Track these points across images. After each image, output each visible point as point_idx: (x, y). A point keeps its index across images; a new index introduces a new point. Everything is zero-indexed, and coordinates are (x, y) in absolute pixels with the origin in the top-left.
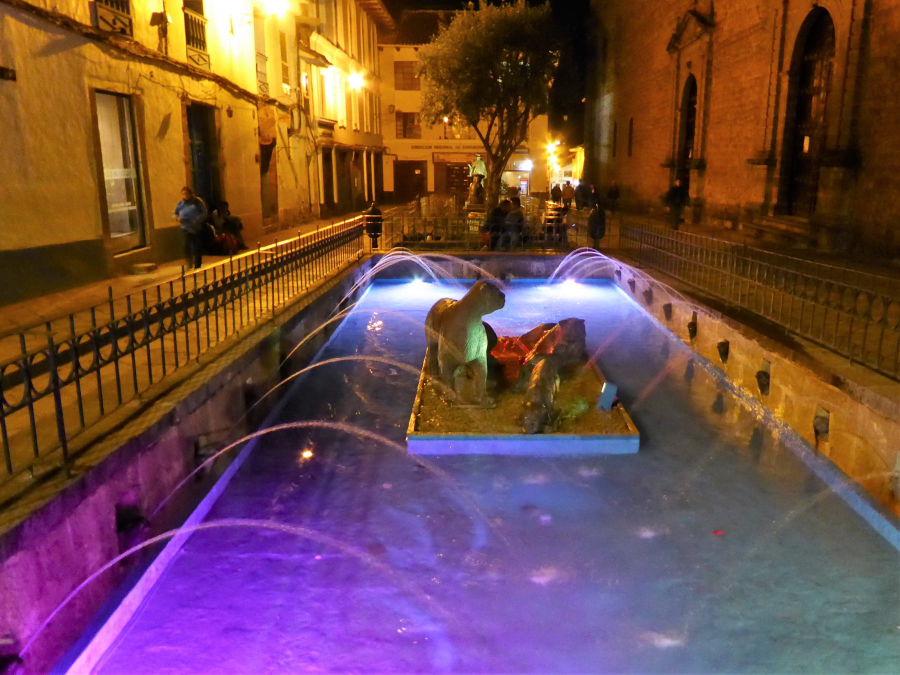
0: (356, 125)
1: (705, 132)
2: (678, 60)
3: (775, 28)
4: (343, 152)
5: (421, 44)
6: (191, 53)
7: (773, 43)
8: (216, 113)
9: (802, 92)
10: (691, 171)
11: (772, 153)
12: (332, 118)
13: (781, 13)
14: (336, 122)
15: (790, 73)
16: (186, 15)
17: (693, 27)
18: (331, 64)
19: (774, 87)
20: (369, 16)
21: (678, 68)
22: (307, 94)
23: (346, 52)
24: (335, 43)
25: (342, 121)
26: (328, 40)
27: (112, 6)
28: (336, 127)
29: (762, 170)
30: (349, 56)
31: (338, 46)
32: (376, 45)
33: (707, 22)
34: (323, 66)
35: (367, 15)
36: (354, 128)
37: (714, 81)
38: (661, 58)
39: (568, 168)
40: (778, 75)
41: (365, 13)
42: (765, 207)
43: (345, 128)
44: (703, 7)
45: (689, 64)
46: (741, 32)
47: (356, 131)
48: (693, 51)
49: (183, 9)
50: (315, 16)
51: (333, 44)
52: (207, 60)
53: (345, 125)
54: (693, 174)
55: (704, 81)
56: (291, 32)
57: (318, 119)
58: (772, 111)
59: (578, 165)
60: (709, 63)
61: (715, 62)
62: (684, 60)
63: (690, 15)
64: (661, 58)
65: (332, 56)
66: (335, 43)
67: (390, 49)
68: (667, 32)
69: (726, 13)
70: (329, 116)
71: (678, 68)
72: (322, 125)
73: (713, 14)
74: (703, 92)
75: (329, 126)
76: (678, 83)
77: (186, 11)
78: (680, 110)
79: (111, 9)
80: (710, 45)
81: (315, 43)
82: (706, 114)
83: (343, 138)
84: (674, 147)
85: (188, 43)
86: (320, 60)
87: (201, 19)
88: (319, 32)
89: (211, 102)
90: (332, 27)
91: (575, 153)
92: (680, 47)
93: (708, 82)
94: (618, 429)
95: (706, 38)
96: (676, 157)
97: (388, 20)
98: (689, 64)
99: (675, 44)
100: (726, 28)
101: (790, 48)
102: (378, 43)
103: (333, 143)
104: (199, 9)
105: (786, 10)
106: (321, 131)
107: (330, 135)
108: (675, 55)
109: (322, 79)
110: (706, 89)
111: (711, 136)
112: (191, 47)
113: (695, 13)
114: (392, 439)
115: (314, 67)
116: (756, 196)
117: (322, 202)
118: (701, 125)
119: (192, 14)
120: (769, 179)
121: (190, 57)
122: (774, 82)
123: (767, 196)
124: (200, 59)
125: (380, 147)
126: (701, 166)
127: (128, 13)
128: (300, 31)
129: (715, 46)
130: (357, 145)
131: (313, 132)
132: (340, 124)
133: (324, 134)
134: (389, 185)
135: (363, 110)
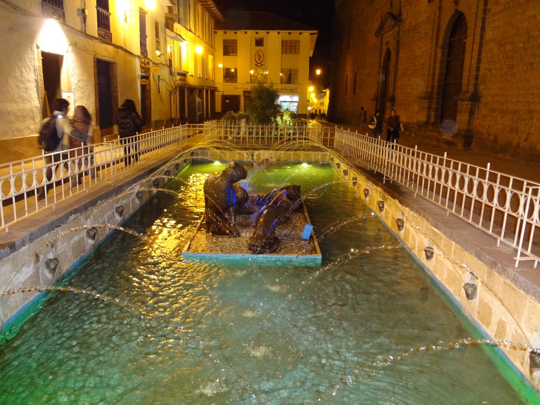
0: (200, 74)
1: (395, 80)
2: (381, 41)
3: (434, 22)
4: (192, 89)
5: (238, 30)
6: (101, 32)
7: (433, 32)
8: (115, 65)
9: (449, 59)
10: (387, 102)
11: (432, 93)
12: (186, 71)
13: (438, 14)
14: (188, 72)
15: (443, 47)
16: (98, 11)
17: (390, 22)
18: (184, 39)
19: (433, 56)
20: (209, 14)
21: (381, 44)
22: (171, 57)
23: (194, 34)
24: (189, 29)
25: (192, 72)
26: (184, 27)
27: (53, 5)
28: (188, 75)
29: (426, 103)
30: (196, 36)
31: (190, 30)
32: (213, 30)
33: (397, 18)
34: (181, 41)
35: (208, 13)
36: (198, 76)
37: (401, 52)
38: (372, 40)
39: (321, 101)
40: (435, 49)
41: (207, 13)
42: (427, 123)
43: (193, 76)
44: (395, 11)
45: (387, 43)
46: (416, 25)
47: (199, 78)
48: (389, 36)
49: (97, 7)
50: (177, 14)
51: (187, 29)
52: (110, 36)
53: (193, 74)
54: (388, 104)
55: (395, 53)
56: (162, 21)
57: (176, 71)
58: (431, 69)
59: (326, 100)
60: (398, 42)
61: (401, 42)
62: (384, 41)
63: (389, 16)
64: (372, 40)
65: (186, 35)
66: (189, 29)
67: (220, 33)
68: (376, 25)
69: (408, 14)
70: (184, 68)
71: (381, 44)
72: (179, 74)
73: (400, 15)
74: (395, 58)
75: (184, 75)
76: (381, 54)
77: (98, 9)
78: (382, 68)
79: (52, 6)
80: (399, 32)
81: (177, 28)
82: (396, 70)
83: (191, 81)
84: (378, 89)
85: (99, 26)
86: (179, 37)
87: (107, 13)
88: (179, 23)
89: (111, 60)
90: (187, 19)
91: (325, 92)
92: (382, 33)
93: (398, 52)
94: (142, 242)
95: (397, 28)
96: (379, 94)
97: (220, 16)
98: (387, 43)
99: (380, 32)
100: (408, 22)
101: (442, 34)
102: (214, 29)
103: (186, 84)
104: (106, 7)
105: (440, 13)
106: (178, 77)
107: (184, 80)
108: (379, 38)
109: (180, 48)
110: (396, 57)
111: (398, 84)
112: (101, 29)
113: (390, 14)
114: (6, 257)
115: (175, 42)
116: (422, 118)
117: (178, 117)
118: (393, 77)
119: (101, 10)
120: (429, 108)
121: (100, 34)
122: (433, 53)
123: (429, 117)
124: (106, 35)
125: (214, 87)
126: (393, 100)
127: (62, 8)
128: (168, 22)
129: (401, 33)
130: (200, 86)
131: (174, 78)
132: (190, 74)
133: (180, 79)
134: (218, 108)
135: (204, 65)
